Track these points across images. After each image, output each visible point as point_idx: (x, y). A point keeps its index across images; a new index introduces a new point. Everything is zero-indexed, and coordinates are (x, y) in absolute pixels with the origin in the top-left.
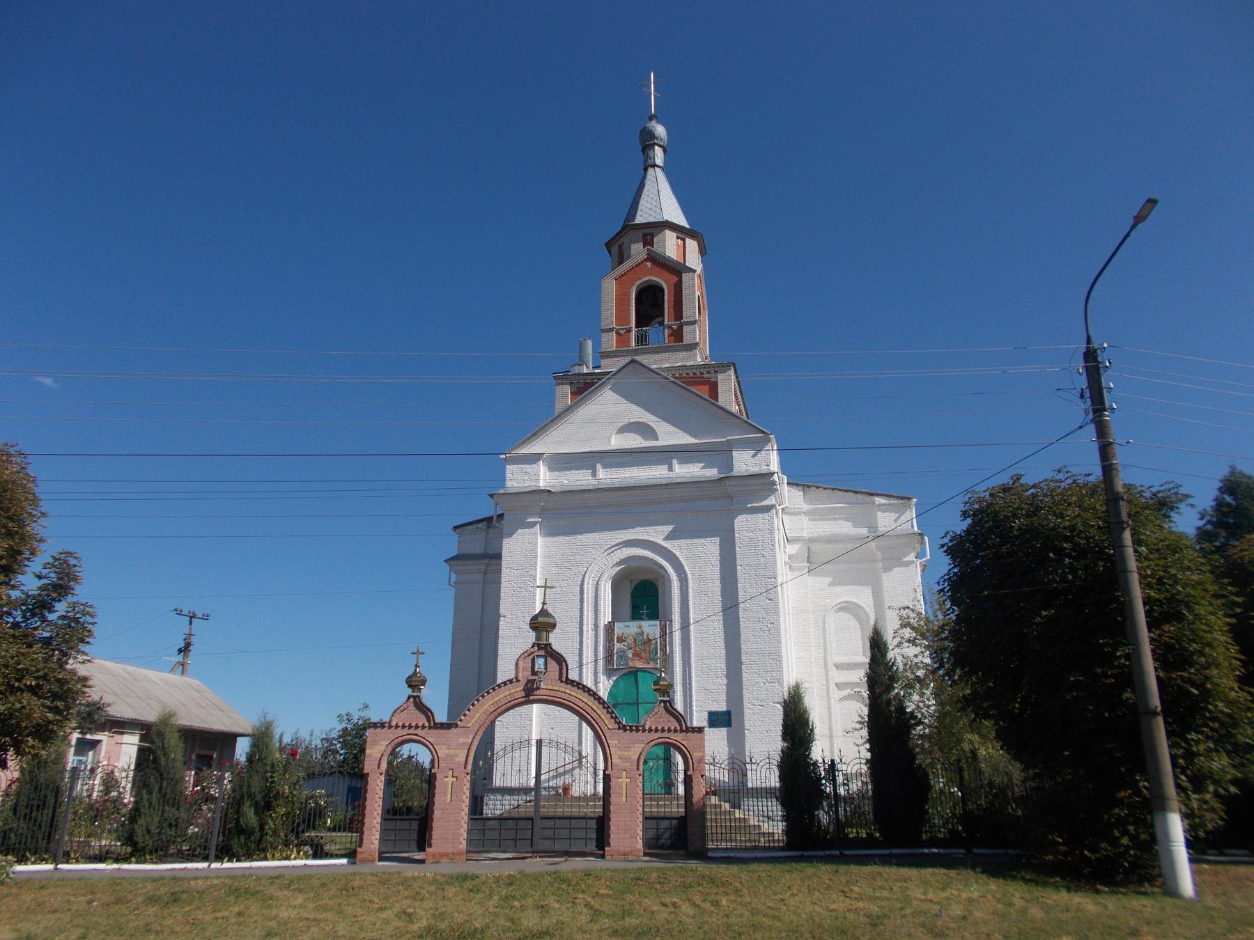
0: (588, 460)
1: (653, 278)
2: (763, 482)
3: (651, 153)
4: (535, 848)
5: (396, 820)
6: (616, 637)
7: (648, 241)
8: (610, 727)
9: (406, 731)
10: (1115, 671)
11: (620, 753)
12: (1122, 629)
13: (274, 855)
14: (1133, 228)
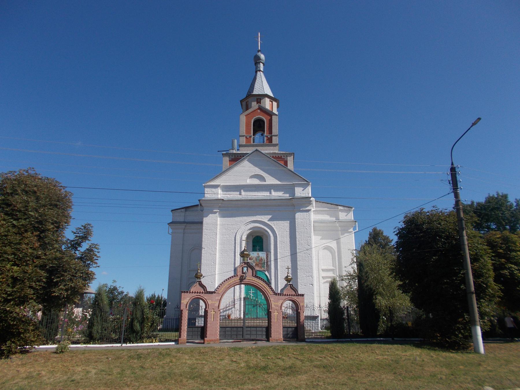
0: (238, 188)
1: (261, 117)
2: (306, 200)
3: (259, 66)
4: (244, 338)
5: (193, 327)
7: (259, 101)
9: (196, 294)
10: (460, 278)
12: (462, 265)
13: (146, 341)
14: (471, 127)
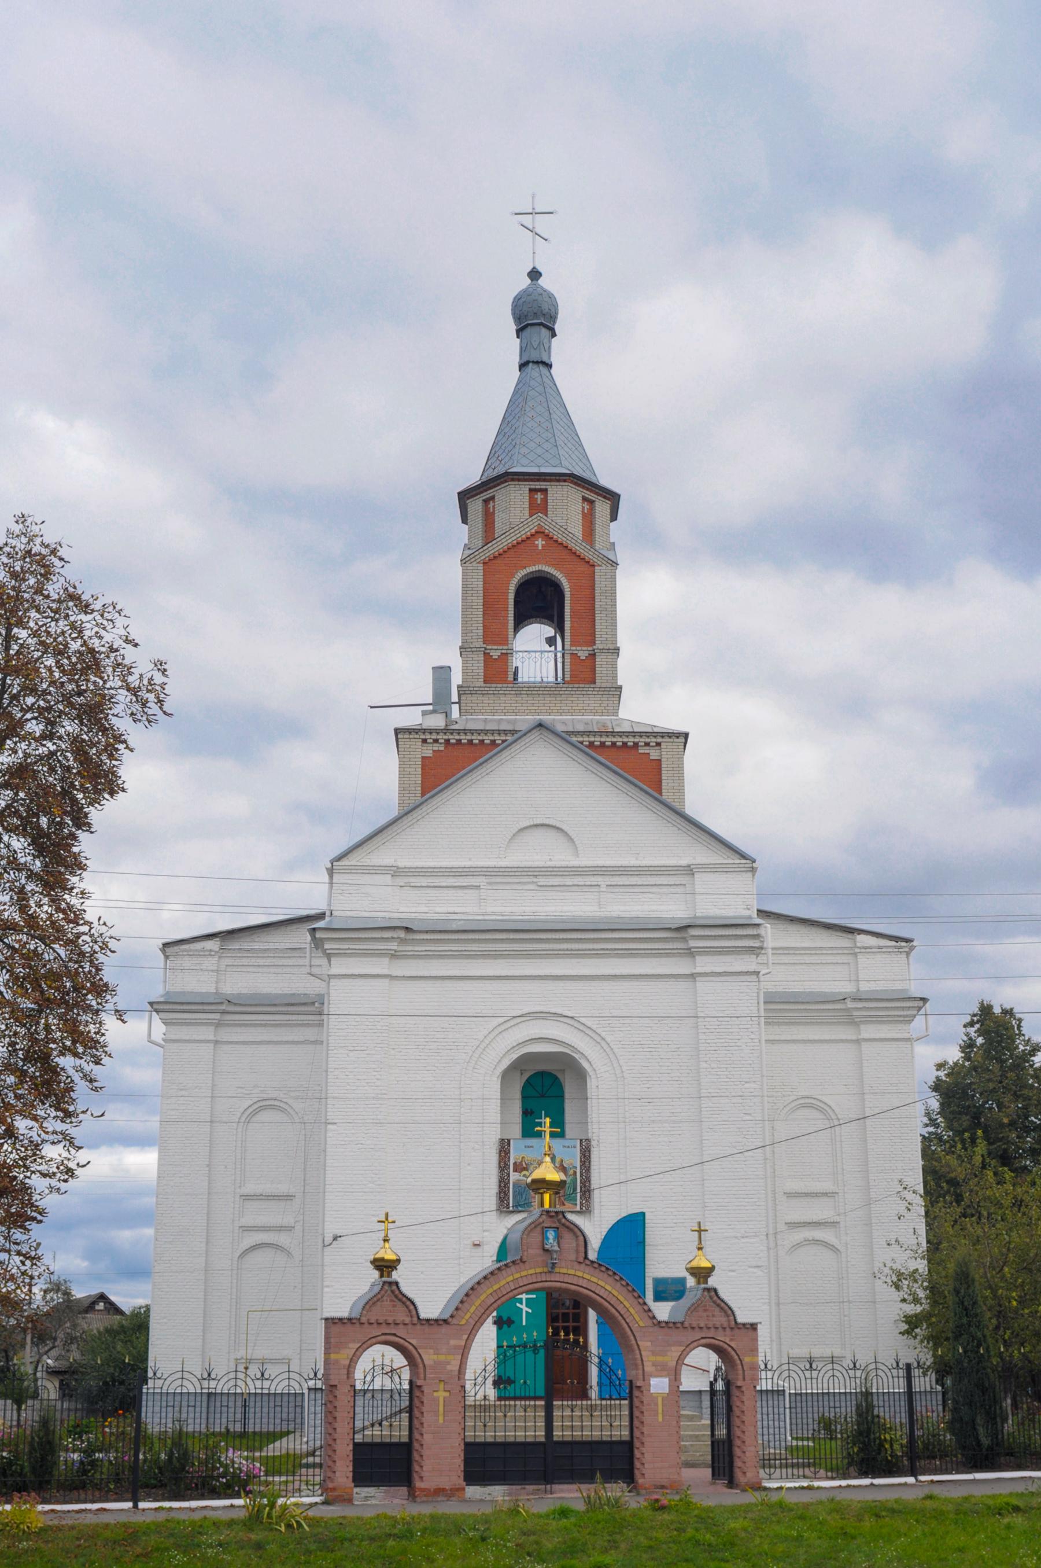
6: (512, 1161)
8: (642, 1324)
11: (653, 1358)
